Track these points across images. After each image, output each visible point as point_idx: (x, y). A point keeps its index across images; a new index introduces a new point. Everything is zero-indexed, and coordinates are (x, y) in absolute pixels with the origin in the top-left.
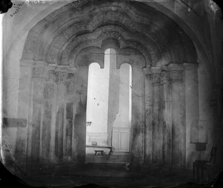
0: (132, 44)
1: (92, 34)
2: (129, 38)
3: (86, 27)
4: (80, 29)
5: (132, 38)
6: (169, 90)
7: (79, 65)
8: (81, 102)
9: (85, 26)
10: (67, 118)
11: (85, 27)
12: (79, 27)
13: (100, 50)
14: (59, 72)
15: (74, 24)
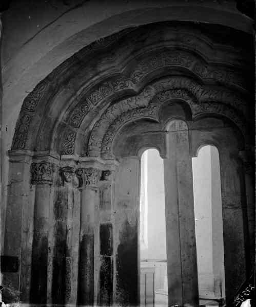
0: (215, 109)
1: (138, 97)
2: (207, 96)
3: (125, 86)
4: (114, 89)
5: (212, 96)
6: (63, 108)
7: (123, 156)
8: (127, 223)
9: (122, 84)
10: (101, 253)
11: (122, 85)
12: (112, 87)
13: (158, 126)
14: (83, 168)
15: (103, 82)
